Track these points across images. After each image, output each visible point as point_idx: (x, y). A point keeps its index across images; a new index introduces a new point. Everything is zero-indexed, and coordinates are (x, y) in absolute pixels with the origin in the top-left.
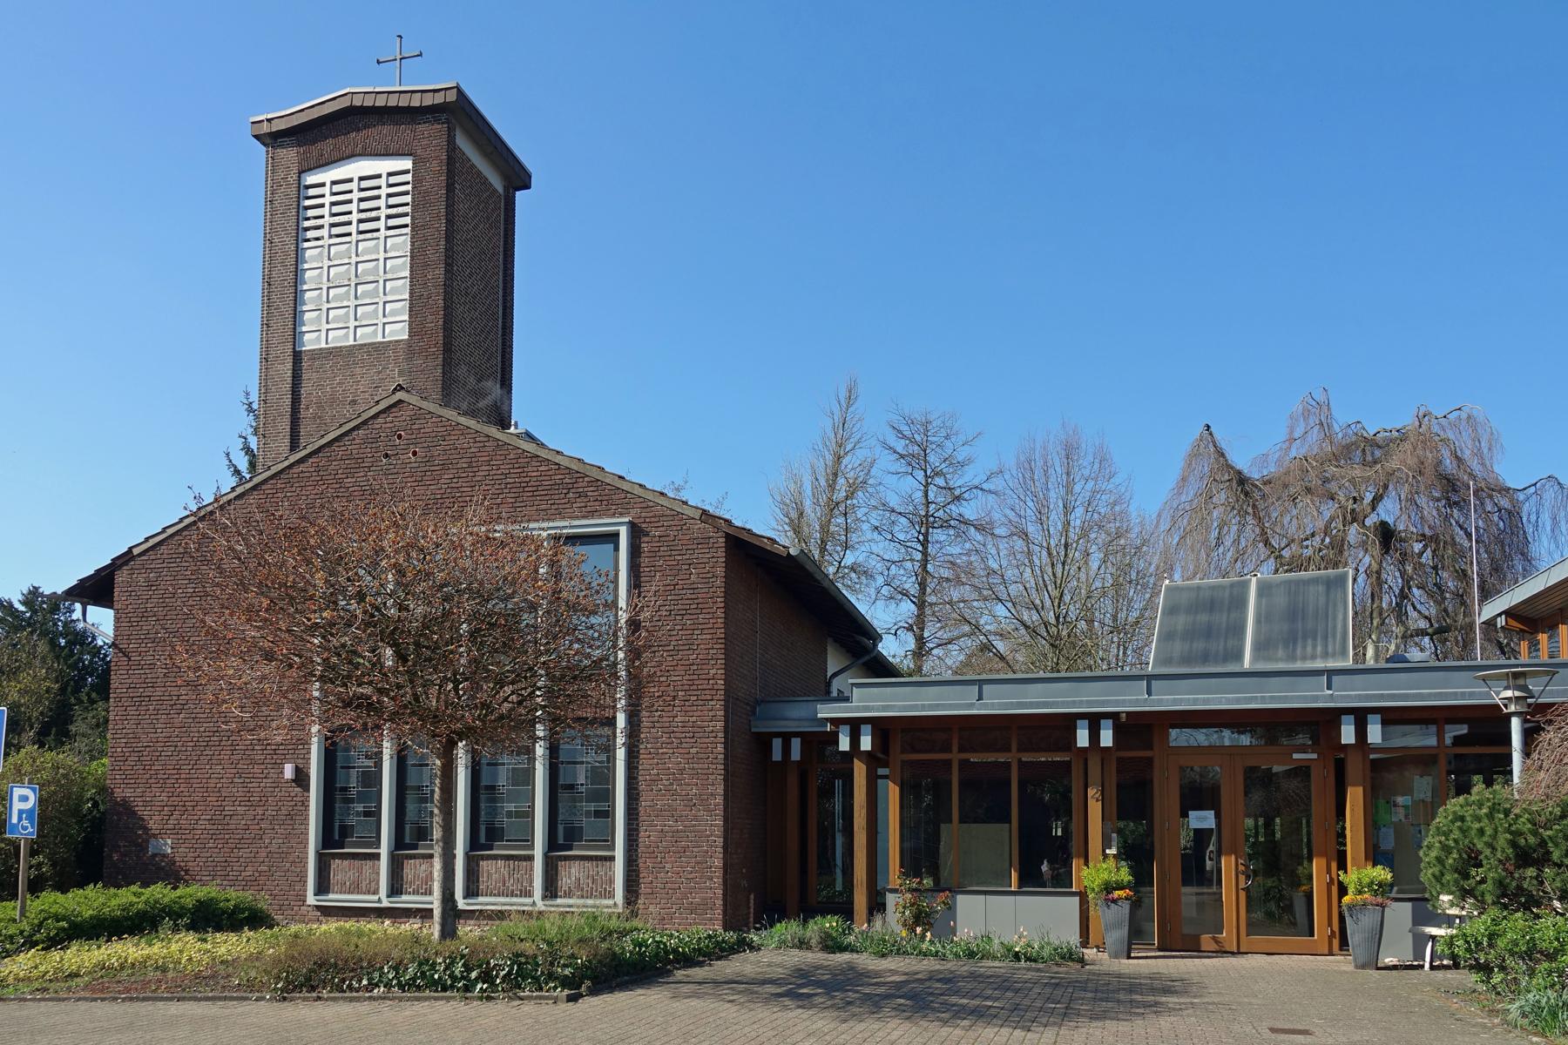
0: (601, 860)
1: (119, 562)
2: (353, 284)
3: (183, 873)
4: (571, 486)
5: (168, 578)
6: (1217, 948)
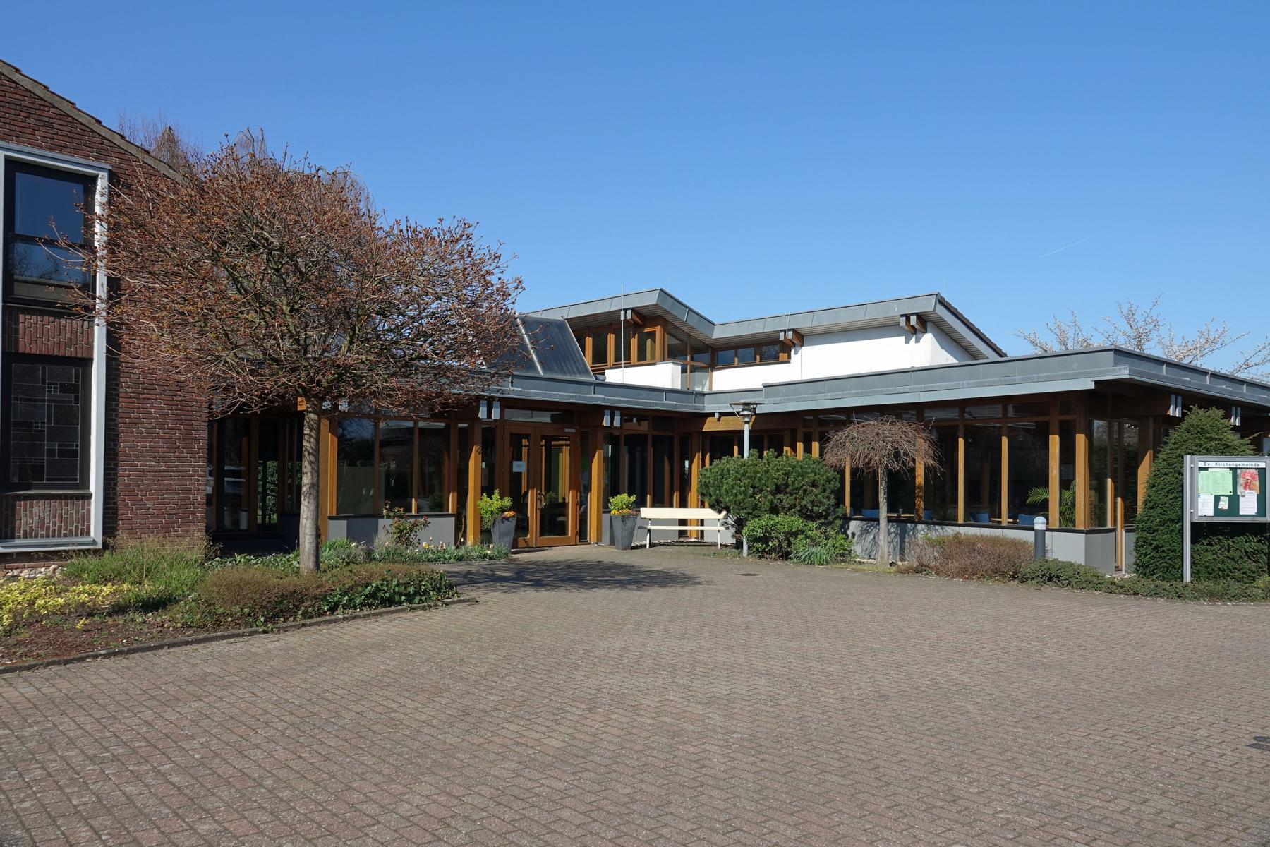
4: (33, 111)
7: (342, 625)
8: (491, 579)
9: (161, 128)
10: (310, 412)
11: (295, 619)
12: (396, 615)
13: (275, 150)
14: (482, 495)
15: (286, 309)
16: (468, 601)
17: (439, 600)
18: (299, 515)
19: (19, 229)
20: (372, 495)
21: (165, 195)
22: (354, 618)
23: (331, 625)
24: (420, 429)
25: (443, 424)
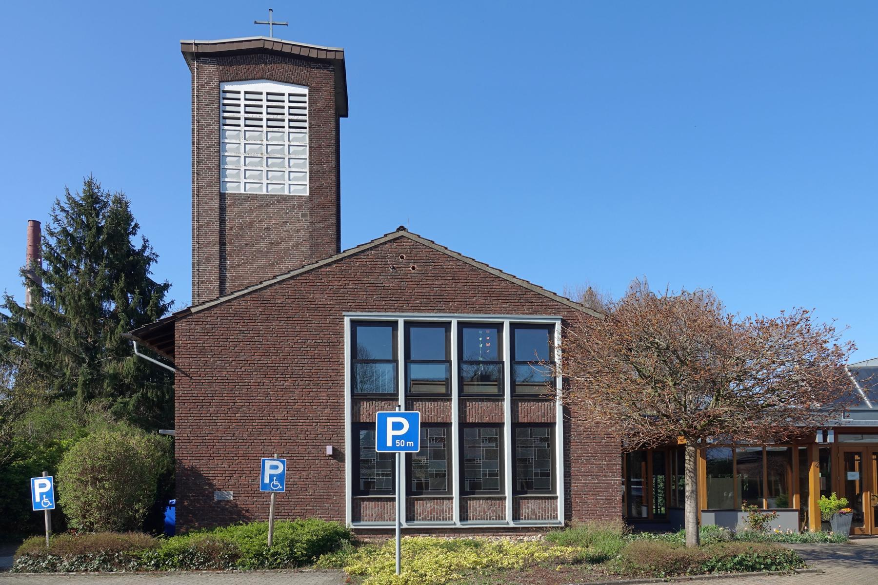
0: (547, 499)
1: (179, 316)
2: (265, 157)
3: (244, 512)
4: (522, 296)
5: (222, 329)
6: (862, 533)
7: (718, 581)
8: (833, 557)
9: (587, 288)
10: (689, 446)
11: (685, 575)
12: (758, 577)
13: (658, 290)
14: (821, 496)
15: (671, 384)
16: (816, 571)
17: (791, 569)
18: (684, 509)
19: (517, 358)
20: (731, 497)
21: (595, 328)
22: (727, 577)
23: (711, 581)
24: (768, 452)
25: (786, 448)
